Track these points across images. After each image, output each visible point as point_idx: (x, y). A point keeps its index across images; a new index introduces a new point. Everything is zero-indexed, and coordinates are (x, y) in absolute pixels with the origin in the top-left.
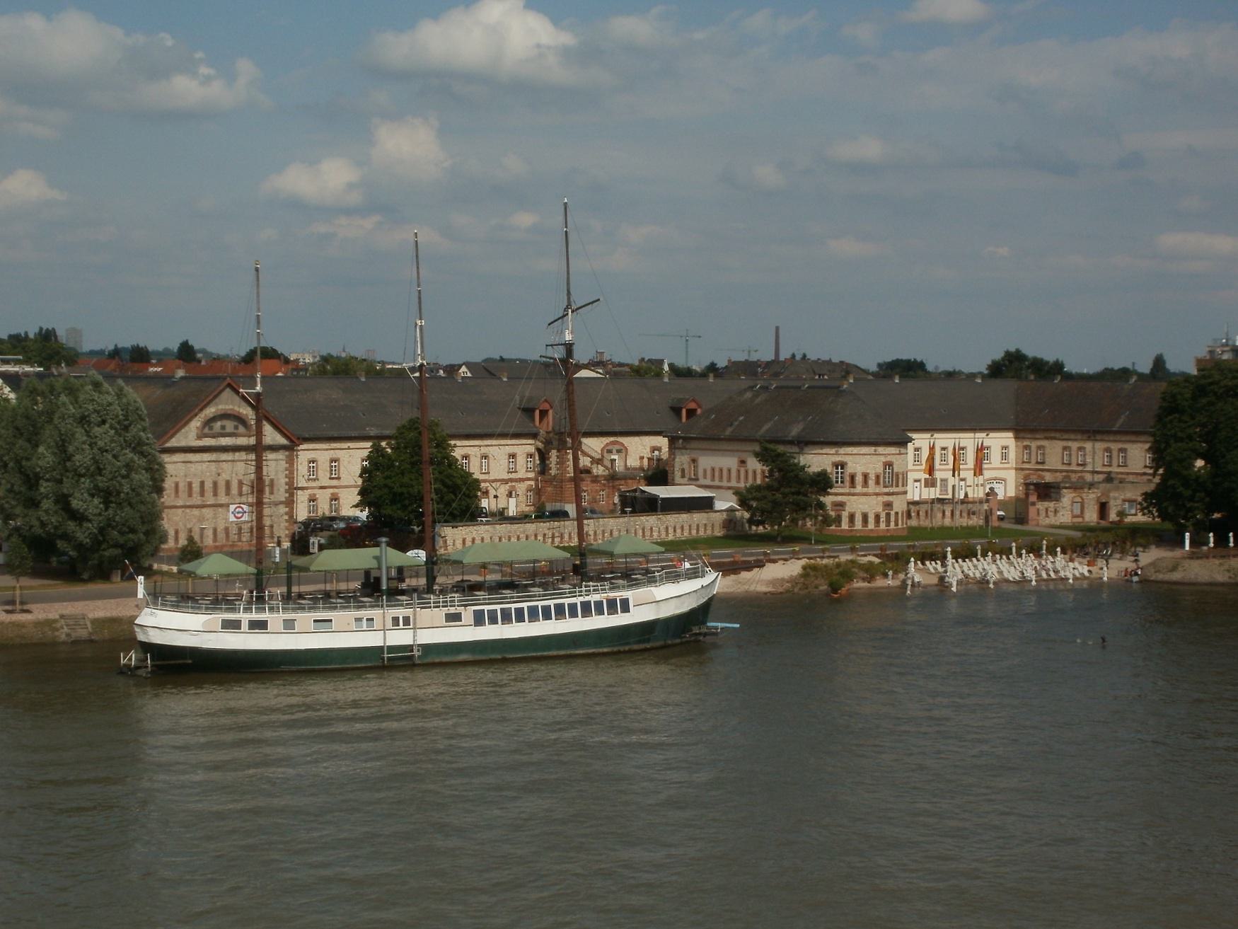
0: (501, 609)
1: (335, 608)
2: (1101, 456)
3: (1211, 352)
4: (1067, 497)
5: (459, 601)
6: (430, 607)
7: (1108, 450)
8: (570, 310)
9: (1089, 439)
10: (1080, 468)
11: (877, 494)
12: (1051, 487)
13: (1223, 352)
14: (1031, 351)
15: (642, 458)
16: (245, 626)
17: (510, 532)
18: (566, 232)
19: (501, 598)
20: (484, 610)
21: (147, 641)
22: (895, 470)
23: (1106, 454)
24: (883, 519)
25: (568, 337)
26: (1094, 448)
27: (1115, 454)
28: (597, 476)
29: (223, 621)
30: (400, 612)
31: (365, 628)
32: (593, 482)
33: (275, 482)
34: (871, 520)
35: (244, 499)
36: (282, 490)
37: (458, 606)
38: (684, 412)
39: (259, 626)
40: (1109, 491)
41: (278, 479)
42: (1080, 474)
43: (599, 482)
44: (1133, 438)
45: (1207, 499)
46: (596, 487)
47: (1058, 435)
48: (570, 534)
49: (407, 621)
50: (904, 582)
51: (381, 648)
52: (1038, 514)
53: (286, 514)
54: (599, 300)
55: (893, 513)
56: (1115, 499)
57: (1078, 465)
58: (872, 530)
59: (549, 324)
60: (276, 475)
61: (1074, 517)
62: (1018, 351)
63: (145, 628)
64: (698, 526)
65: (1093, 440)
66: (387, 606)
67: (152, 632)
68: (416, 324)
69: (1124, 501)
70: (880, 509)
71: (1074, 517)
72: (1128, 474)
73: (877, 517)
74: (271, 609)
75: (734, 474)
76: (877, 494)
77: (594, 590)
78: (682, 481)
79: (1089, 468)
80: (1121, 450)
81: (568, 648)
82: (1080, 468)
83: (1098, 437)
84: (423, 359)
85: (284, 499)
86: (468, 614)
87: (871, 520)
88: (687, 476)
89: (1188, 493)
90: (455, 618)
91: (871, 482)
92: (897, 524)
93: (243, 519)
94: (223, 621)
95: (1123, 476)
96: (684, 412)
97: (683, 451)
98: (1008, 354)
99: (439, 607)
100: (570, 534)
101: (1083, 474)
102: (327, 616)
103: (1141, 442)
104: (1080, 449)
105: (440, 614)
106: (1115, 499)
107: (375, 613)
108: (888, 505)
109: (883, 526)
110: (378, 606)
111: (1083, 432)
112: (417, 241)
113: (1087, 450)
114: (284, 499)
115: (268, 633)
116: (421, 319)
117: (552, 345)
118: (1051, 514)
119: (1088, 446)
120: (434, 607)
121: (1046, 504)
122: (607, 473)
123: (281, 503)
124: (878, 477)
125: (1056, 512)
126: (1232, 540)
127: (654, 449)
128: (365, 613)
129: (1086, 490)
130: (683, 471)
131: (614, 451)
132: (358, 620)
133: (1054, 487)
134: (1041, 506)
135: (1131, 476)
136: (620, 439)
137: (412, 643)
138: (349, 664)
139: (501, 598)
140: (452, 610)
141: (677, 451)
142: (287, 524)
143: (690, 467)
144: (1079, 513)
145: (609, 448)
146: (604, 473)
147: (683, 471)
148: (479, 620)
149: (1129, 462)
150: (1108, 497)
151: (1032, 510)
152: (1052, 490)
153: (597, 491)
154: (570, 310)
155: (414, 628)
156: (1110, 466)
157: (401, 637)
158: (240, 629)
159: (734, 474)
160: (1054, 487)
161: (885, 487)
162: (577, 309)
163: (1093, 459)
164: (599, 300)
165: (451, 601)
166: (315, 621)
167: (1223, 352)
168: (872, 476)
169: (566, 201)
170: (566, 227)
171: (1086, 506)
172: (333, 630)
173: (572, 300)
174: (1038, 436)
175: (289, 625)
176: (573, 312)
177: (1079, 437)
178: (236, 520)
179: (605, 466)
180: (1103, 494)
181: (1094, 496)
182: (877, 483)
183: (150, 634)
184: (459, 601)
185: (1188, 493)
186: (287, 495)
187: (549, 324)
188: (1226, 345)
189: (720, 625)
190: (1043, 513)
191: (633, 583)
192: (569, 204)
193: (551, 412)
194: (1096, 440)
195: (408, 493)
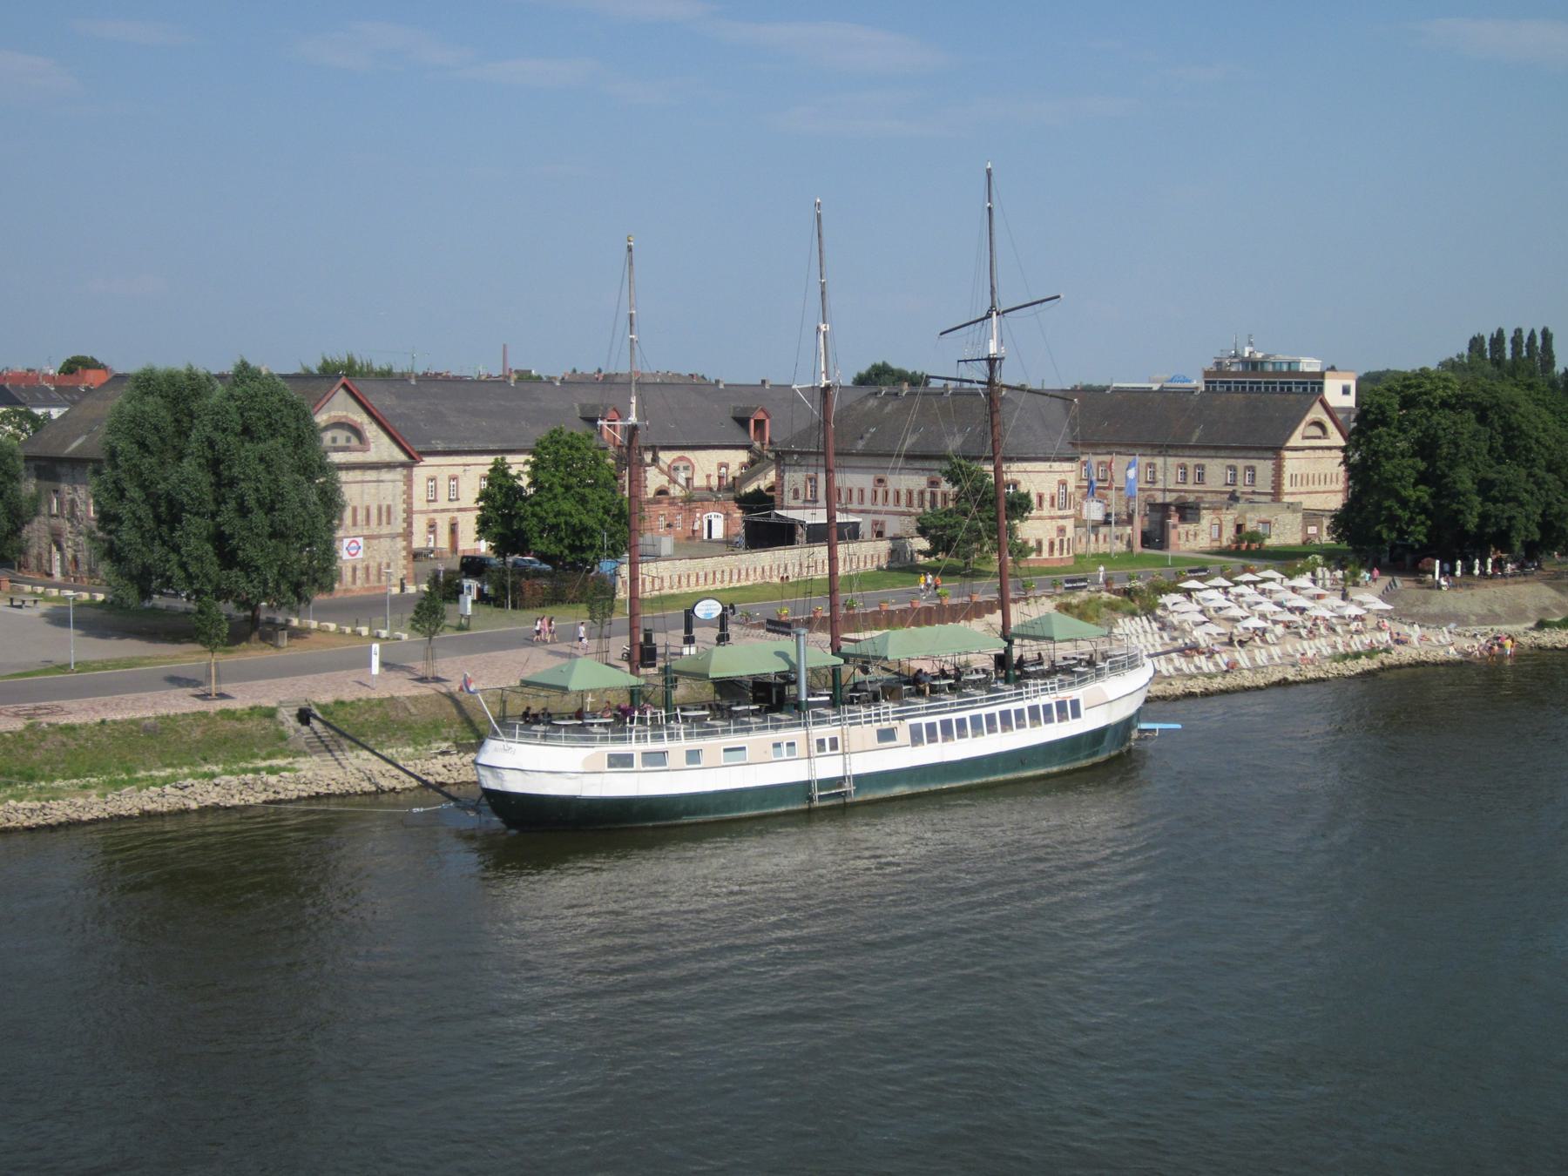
0: (941, 722)
1: (748, 730)
2: (1174, 473)
3: (1218, 364)
4: (1207, 517)
5: (894, 712)
6: (860, 724)
7: (1183, 466)
8: (994, 313)
9: (1160, 454)
10: (1148, 486)
11: (1052, 518)
12: (1186, 508)
13: (1231, 363)
14: (895, 365)
15: (708, 476)
16: (637, 760)
17: (689, 569)
18: (990, 208)
19: (941, 706)
20: (921, 724)
21: (499, 788)
22: (1068, 490)
23: (1248, 473)
24: (1057, 546)
25: (993, 348)
26: (1165, 464)
27: (1240, 472)
28: (674, 498)
29: (610, 756)
30: (825, 732)
31: (785, 757)
32: (672, 504)
33: (392, 510)
34: (1046, 547)
35: (358, 531)
36: (400, 519)
37: (893, 719)
38: (752, 422)
39: (656, 760)
40: (1246, 512)
41: (396, 505)
42: (1149, 493)
43: (675, 504)
44: (1212, 453)
45: (1429, 523)
46: (673, 510)
47: (1122, 450)
48: (747, 570)
49: (834, 744)
50: (28, 459)
51: (808, 784)
52: (1179, 538)
53: (404, 548)
54: (1058, 297)
55: (1065, 539)
56: (1251, 520)
57: (1147, 482)
58: (1046, 559)
59: (942, 334)
60: (393, 500)
61: (1213, 540)
62: (885, 364)
63: (499, 770)
64: (865, 557)
65: (1164, 456)
66: (814, 724)
67: (508, 775)
68: (818, 328)
69: (1259, 522)
70: (1054, 534)
71: (1213, 540)
72: (1206, 492)
73: (1052, 545)
74: (671, 736)
75: (868, 495)
76: (1052, 518)
77: (1042, 690)
78: (793, 503)
79: (1160, 485)
80: (1197, 466)
81: (1015, 769)
82: (1148, 486)
83: (1171, 452)
84: (827, 378)
85: (401, 531)
86: (903, 731)
87: (1046, 547)
88: (802, 497)
89: (1406, 515)
90: (886, 735)
91: (1046, 504)
92: (1068, 553)
93: (358, 556)
94: (610, 756)
95: (1200, 495)
96: (752, 422)
97: (796, 468)
98: (874, 367)
99: (870, 722)
100: (747, 570)
101: (1153, 493)
102: (740, 742)
103: (1222, 457)
104: (1150, 465)
105: (871, 730)
106: (1251, 520)
107: (796, 734)
108: (1062, 530)
109: (1056, 554)
110: (800, 725)
111: (1153, 447)
112: (819, 216)
113: (1158, 467)
114: (401, 531)
115: (668, 770)
116: (824, 322)
117: (966, 361)
118: (1191, 537)
119: (1159, 461)
120: (866, 722)
121: (1187, 526)
122: (683, 494)
123: (399, 535)
124: (1053, 498)
125: (1196, 535)
126: (1459, 568)
127: (721, 465)
128: (784, 735)
129: (1224, 511)
130: (796, 492)
131: (681, 469)
132: (777, 745)
133: (1191, 508)
134: (1183, 528)
135: (1209, 495)
136: (688, 454)
137: (841, 774)
138: (768, 807)
139: (941, 706)
140: (885, 725)
141: (787, 468)
142: (405, 562)
143: (806, 487)
144: (1217, 536)
145: (676, 465)
146: (681, 494)
147: (796, 492)
148: (916, 737)
149: (1207, 479)
150: (1245, 518)
151: (1173, 535)
152: (1188, 511)
153: (674, 515)
154: (994, 313)
155: (843, 754)
156: (1184, 483)
157: (828, 767)
158: (632, 766)
159: (868, 495)
160: (1191, 508)
161: (1060, 509)
162: (1004, 312)
163: (1165, 475)
164: (1058, 297)
165: (885, 714)
166: (725, 750)
167: (1231, 363)
168: (1047, 498)
169: (989, 166)
170: (989, 201)
171: (1224, 528)
172: (747, 761)
173: (996, 299)
174: (1099, 451)
175: (693, 756)
176: (998, 314)
177: (1149, 452)
178: (350, 558)
179: (680, 485)
180: (1240, 516)
181: (1231, 517)
182: (1052, 505)
183: (507, 778)
184: (894, 712)
185: (1406, 515)
186: (405, 525)
187: (942, 334)
188: (1235, 357)
189: (1157, 726)
190: (1183, 537)
191: (1083, 679)
192: (993, 171)
193: (767, 421)
194: (1170, 456)
195: (566, 523)
